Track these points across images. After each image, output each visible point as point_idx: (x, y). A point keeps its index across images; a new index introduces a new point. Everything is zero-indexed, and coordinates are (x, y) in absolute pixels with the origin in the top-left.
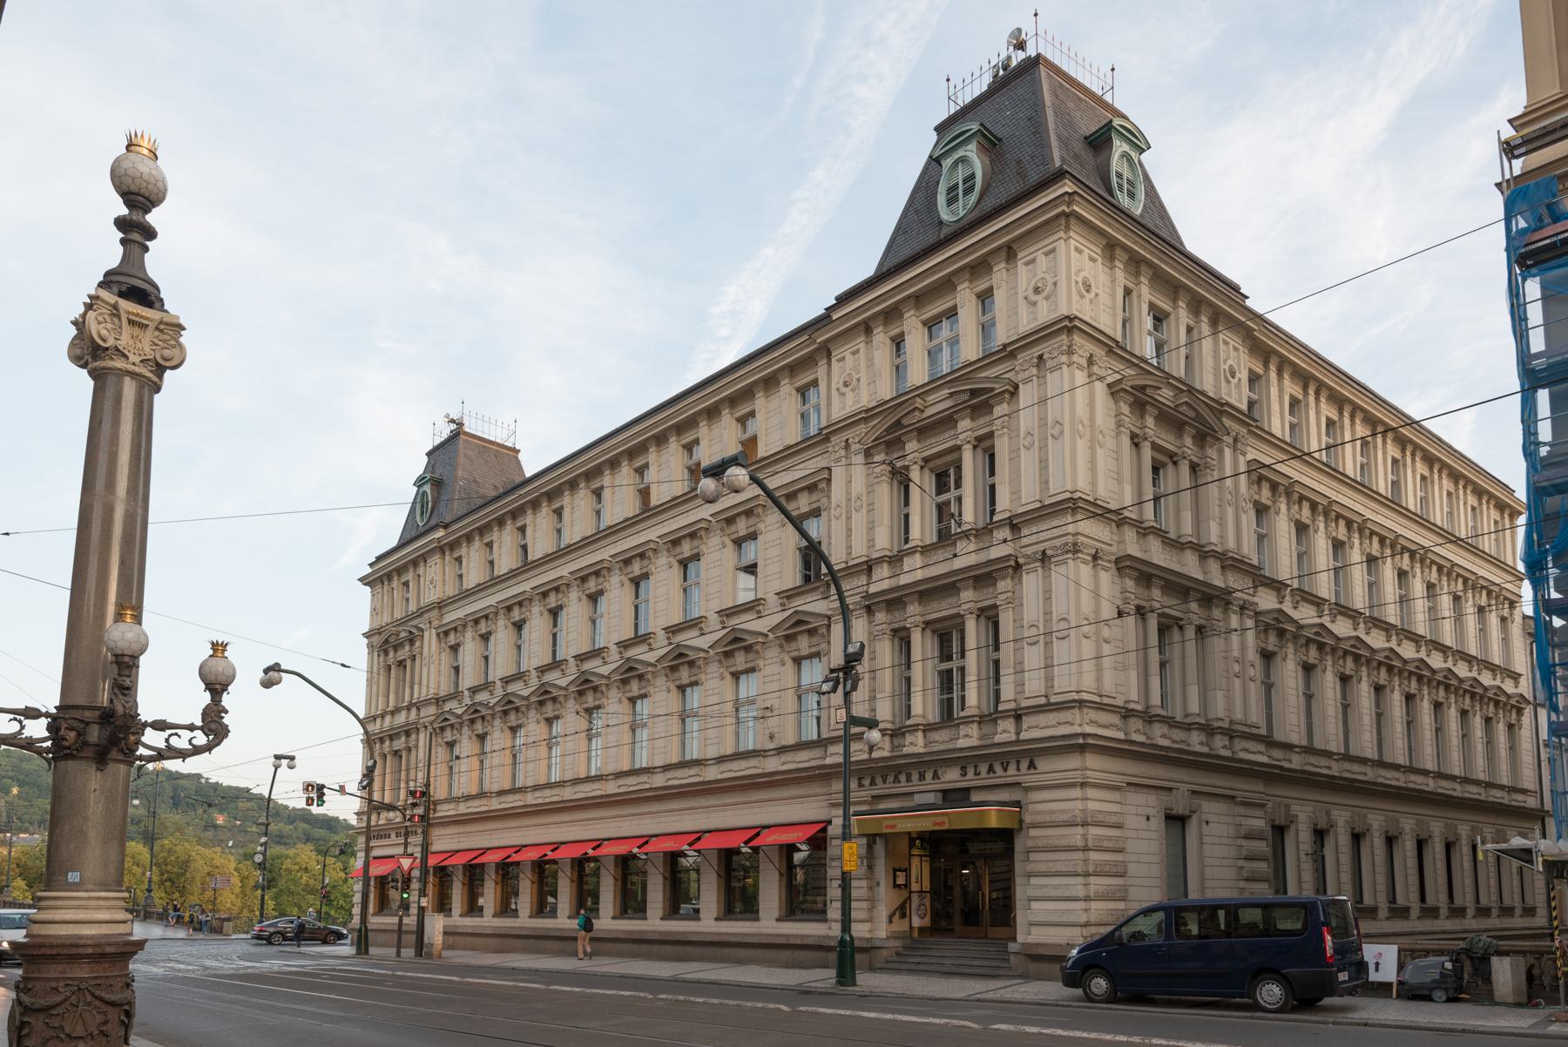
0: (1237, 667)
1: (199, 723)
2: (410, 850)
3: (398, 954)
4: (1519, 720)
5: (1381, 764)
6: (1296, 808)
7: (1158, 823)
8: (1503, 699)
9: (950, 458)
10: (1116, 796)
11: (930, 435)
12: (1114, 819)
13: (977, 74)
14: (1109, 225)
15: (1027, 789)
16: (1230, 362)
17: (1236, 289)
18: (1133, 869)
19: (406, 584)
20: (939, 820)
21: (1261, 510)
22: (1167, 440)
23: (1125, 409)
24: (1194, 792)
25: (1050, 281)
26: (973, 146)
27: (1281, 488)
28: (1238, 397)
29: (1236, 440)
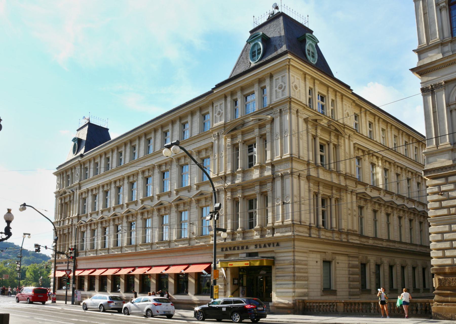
1: (4, 232)
2: (69, 268)
3: (66, 303)
5: (400, 242)
6: (369, 258)
7: (320, 264)
10: (306, 255)
11: (246, 136)
12: (304, 262)
14: (303, 68)
15: (276, 253)
16: (347, 111)
17: (348, 87)
18: (310, 279)
19: (68, 176)
21: (359, 159)
22: (326, 137)
23: (310, 127)
24: (333, 253)
25: (284, 85)
26: (260, 39)
28: (351, 122)
29: (349, 136)
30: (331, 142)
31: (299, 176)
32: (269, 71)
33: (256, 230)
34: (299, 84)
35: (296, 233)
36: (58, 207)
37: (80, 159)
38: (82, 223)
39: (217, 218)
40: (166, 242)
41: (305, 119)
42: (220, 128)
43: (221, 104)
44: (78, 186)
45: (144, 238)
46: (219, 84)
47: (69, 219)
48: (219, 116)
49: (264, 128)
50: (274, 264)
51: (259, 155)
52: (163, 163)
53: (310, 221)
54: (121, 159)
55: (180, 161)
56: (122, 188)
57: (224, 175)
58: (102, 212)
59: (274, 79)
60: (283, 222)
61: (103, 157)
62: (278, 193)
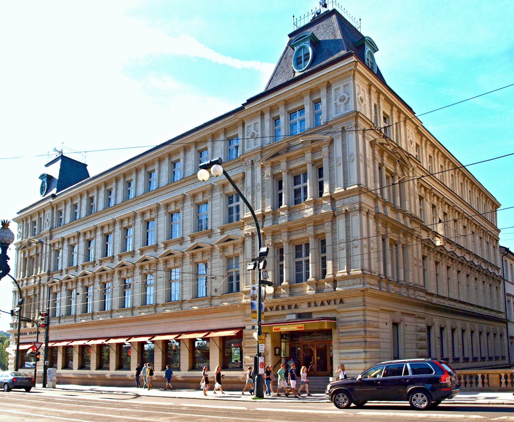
0: (415, 262)
4: (499, 286)
7: (390, 326)
8: (495, 277)
9: (301, 169)
10: (376, 314)
12: (376, 324)
13: (302, 17)
15: (338, 313)
16: (410, 138)
20: (303, 325)
21: (421, 198)
24: (402, 313)
25: (347, 97)
26: (308, 42)
27: (428, 190)
28: (413, 152)
29: (413, 170)
30: (396, 174)
31: (367, 213)
32: (325, 79)
33: (310, 284)
34: (364, 97)
35: (368, 286)
36: (19, 262)
37: (51, 200)
38: (54, 282)
39: (264, 267)
40: (150, 306)
41: (371, 142)
42: (255, 154)
43: (255, 124)
44: (48, 234)
45: (144, 298)
46: (251, 99)
47: (35, 278)
48: (342, 103)
49: (319, 153)
50: (335, 326)
51: (312, 188)
52: (172, 202)
53: (379, 271)
54: (110, 199)
55: (145, 215)
56: (76, 247)
57: (262, 214)
58: (67, 271)
59: (333, 89)
60: (348, 272)
61: (85, 196)
62: (341, 235)
